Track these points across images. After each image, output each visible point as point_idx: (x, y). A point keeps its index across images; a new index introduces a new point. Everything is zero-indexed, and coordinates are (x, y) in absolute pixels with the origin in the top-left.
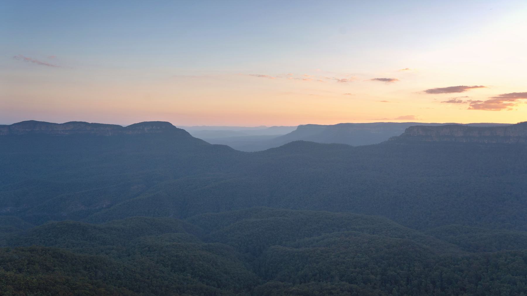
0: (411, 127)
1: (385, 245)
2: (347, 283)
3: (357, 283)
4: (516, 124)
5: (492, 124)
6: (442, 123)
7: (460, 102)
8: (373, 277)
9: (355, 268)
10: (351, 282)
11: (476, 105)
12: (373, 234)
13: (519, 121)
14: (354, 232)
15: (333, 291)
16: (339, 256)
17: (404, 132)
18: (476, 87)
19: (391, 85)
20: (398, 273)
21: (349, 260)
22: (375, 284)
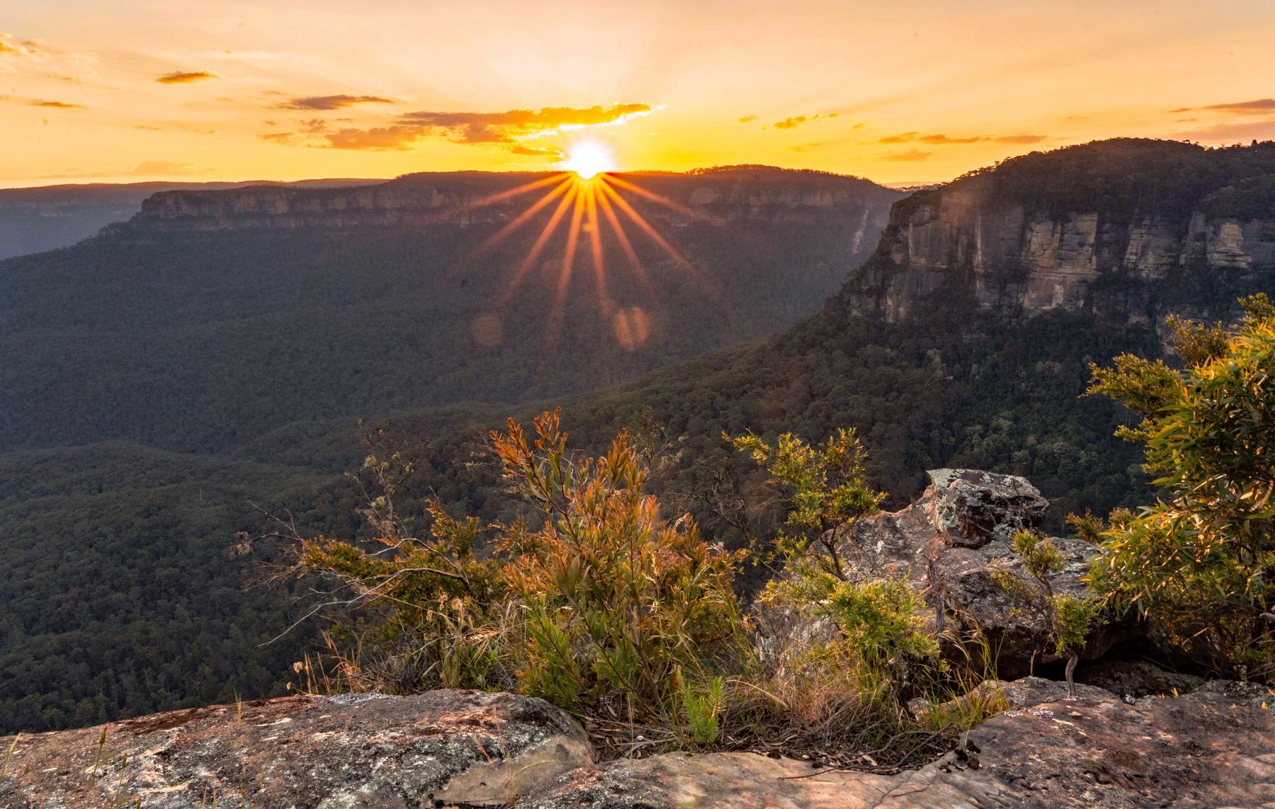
0: (158, 194)
1: (138, 509)
2: (51, 635)
3: (78, 626)
4: (392, 182)
5: (368, 180)
6: (236, 181)
7: (1005, 140)
8: (118, 596)
9: (67, 590)
10: (58, 628)
11: (342, 140)
12: (100, 491)
13: (399, 174)
14: (43, 499)
15: (13, 670)
16: (10, 576)
17: (139, 210)
18: (374, 99)
19: (197, 83)
20: (183, 568)
21: (43, 575)
22: (128, 612)
